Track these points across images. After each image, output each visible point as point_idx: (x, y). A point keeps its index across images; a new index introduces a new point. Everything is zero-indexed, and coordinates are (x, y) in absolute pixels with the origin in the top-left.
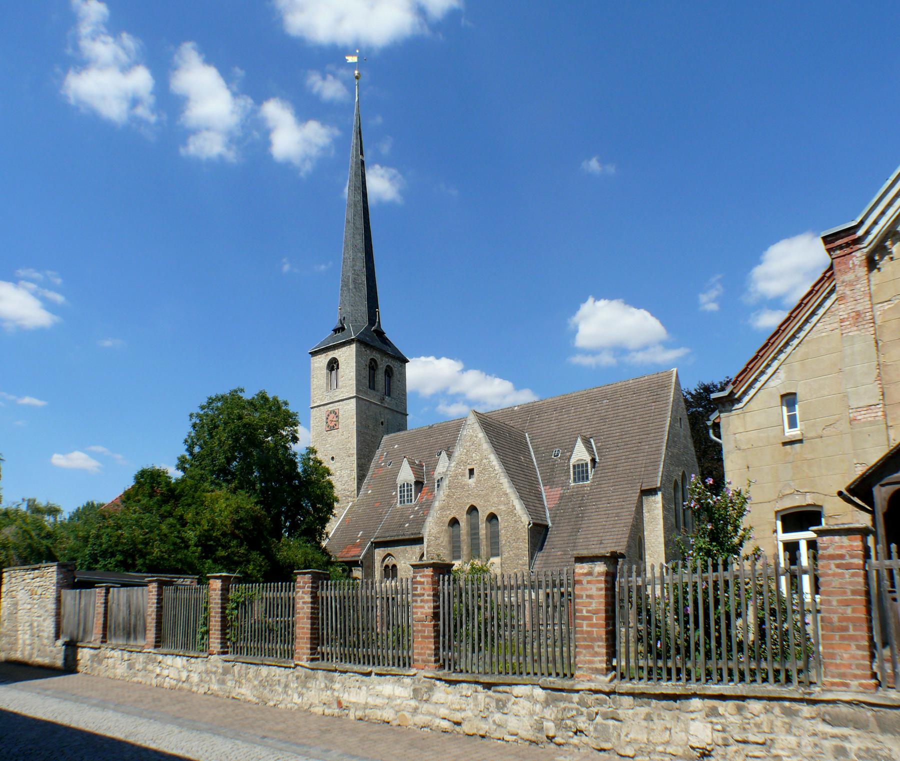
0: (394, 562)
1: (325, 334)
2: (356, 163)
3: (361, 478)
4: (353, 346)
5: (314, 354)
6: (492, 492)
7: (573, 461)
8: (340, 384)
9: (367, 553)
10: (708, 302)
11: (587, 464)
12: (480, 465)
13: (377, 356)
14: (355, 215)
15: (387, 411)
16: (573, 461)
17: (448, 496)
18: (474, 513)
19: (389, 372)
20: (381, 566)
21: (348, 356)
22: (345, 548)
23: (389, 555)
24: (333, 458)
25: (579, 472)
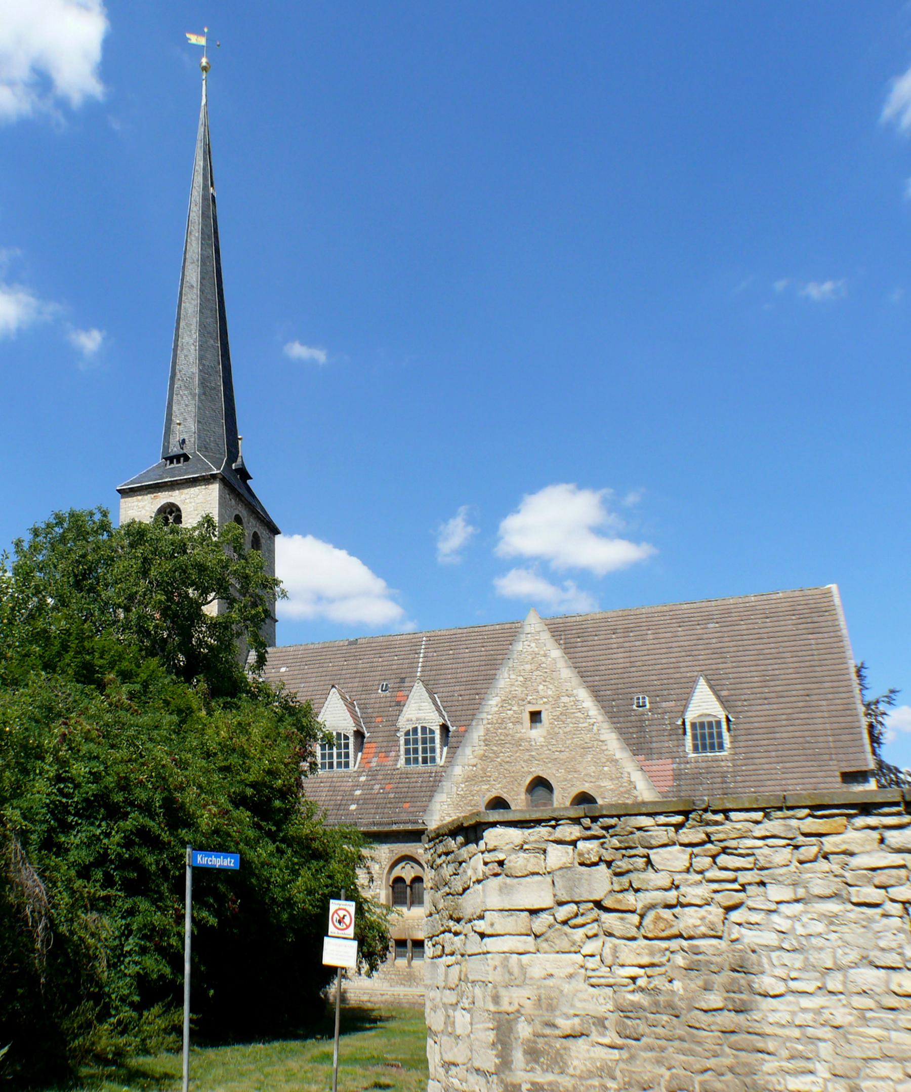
1: (150, 464)
4: (215, 489)
5: (126, 493)
10: (456, 535)
11: (719, 723)
12: (556, 705)
14: (202, 278)
16: (691, 716)
17: (484, 757)
18: (541, 792)
19: (256, 542)
20: (388, 879)
25: (703, 737)
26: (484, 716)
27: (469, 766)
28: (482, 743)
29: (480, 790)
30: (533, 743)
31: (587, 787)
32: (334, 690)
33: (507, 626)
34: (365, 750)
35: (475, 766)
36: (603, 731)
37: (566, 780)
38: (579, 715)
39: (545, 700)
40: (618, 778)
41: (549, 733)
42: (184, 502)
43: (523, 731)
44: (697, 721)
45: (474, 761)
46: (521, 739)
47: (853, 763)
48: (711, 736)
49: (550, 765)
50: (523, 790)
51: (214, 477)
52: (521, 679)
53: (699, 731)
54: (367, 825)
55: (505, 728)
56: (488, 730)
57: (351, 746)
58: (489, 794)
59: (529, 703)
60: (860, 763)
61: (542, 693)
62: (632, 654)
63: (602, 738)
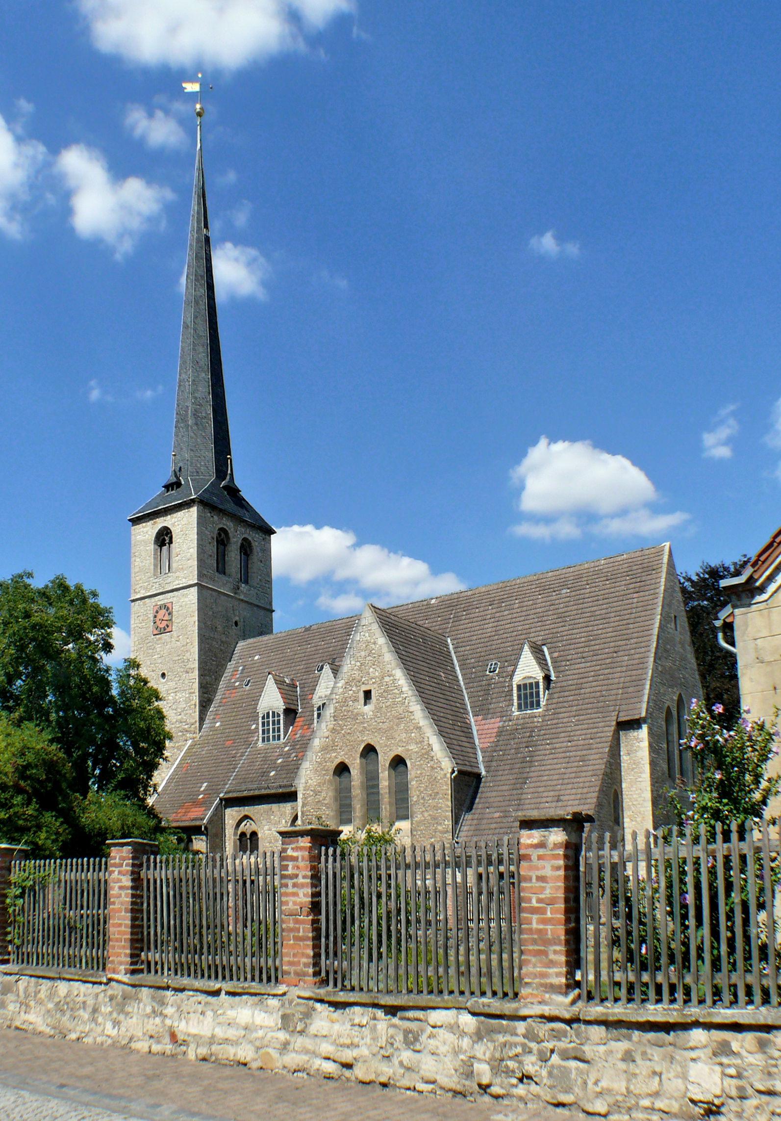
0: (254, 827)
2: (198, 241)
3: (205, 704)
4: (194, 510)
5: (136, 521)
6: (398, 725)
7: (517, 679)
11: (537, 684)
12: (380, 685)
13: (228, 524)
15: (243, 605)
16: (517, 679)
17: (333, 731)
19: (246, 548)
20: (235, 834)
21: (185, 525)
22: (181, 807)
23: (246, 817)
24: (163, 675)
25: (525, 695)
28: (332, 719)
31: (399, 751)
32: (270, 676)
33: (417, 605)
34: (296, 724)
35: (327, 738)
36: (411, 704)
37: (386, 746)
38: (396, 691)
40: (421, 742)
41: (376, 708)
42: (173, 525)
44: (521, 683)
45: (326, 734)
46: (357, 714)
47: (631, 712)
48: (531, 694)
50: (359, 756)
51: (193, 501)
52: (358, 664)
53: (522, 692)
54: (276, 788)
57: (282, 722)
60: (636, 712)
61: (371, 675)
62: (500, 623)
63: (411, 709)
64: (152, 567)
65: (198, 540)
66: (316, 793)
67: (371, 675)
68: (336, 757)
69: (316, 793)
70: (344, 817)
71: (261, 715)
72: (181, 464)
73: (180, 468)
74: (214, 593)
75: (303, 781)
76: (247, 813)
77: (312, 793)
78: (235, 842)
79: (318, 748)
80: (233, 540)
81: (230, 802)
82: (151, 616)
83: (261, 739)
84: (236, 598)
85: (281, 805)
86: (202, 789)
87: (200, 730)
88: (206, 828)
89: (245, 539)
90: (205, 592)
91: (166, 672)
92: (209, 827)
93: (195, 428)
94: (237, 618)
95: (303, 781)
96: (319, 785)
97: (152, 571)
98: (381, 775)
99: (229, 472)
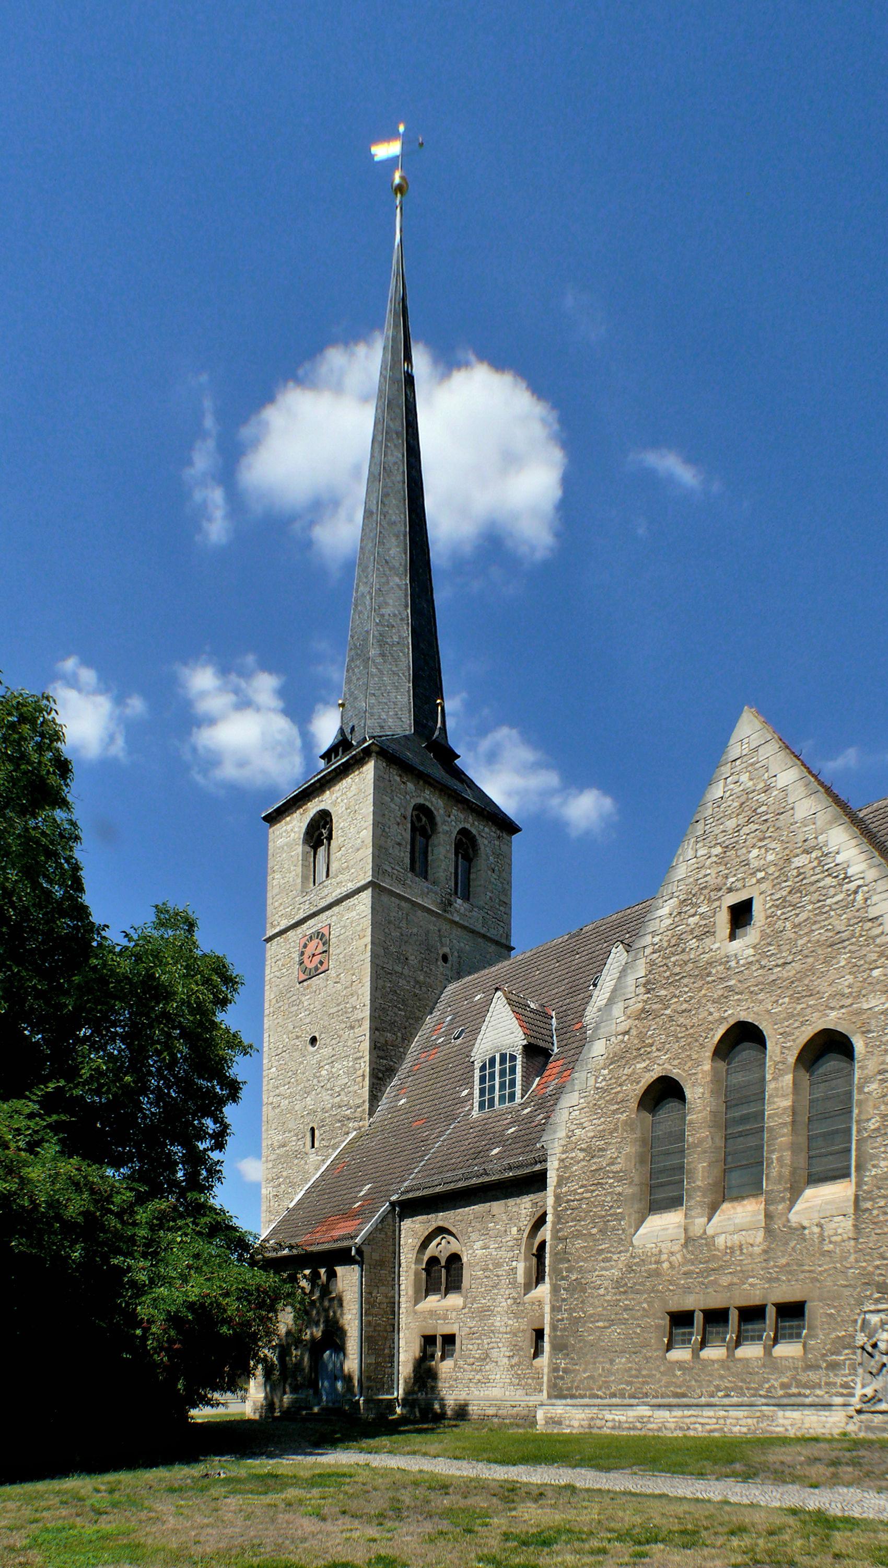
0: (455, 1246)
2: (393, 380)
3: (381, 1075)
8: (334, 866)
9: (376, 1230)
13: (437, 803)
15: (457, 932)
17: (644, 1014)
19: (466, 846)
20: (418, 1261)
21: (354, 802)
22: (321, 1223)
23: (441, 1231)
24: (313, 1041)
26: (648, 940)
27: (616, 1035)
29: (634, 1072)
30: (733, 964)
31: (832, 1020)
32: (499, 993)
34: (547, 1073)
38: (829, 881)
39: (760, 875)
42: (335, 803)
43: (717, 945)
49: (760, 997)
50: (709, 1054)
52: (718, 850)
55: (683, 951)
56: (652, 963)
57: (519, 1069)
58: (648, 1075)
59: (730, 890)
61: (755, 864)
63: (873, 912)
64: (299, 880)
65: (374, 813)
66: (591, 1153)
67: (755, 864)
68: (647, 1069)
69: (591, 1153)
70: (660, 1195)
71: (478, 1065)
72: (355, 722)
73: (353, 729)
74: (403, 904)
75: (562, 1133)
76: (441, 1224)
77: (581, 1155)
78: (416, 1274)
79: (601, 1061)
80: (442, 828)
81: (411, 1207)
82: (296, 956)
83: (476, 1105)
84: (446, 919)
85: (511, 1202)
86: (362, 1194)
87: (371, 1114)
88: (359, 1251)
89: (464, 832)
90: (385, 898)
91: (317, 1035)
92: (365, 1249)
93: (379, 660)
94: (446, 950)
95: (562, 1133)
96: (601, 1136)
97: (299, 887)
98: (770, 1087)
99: (439, 725)
